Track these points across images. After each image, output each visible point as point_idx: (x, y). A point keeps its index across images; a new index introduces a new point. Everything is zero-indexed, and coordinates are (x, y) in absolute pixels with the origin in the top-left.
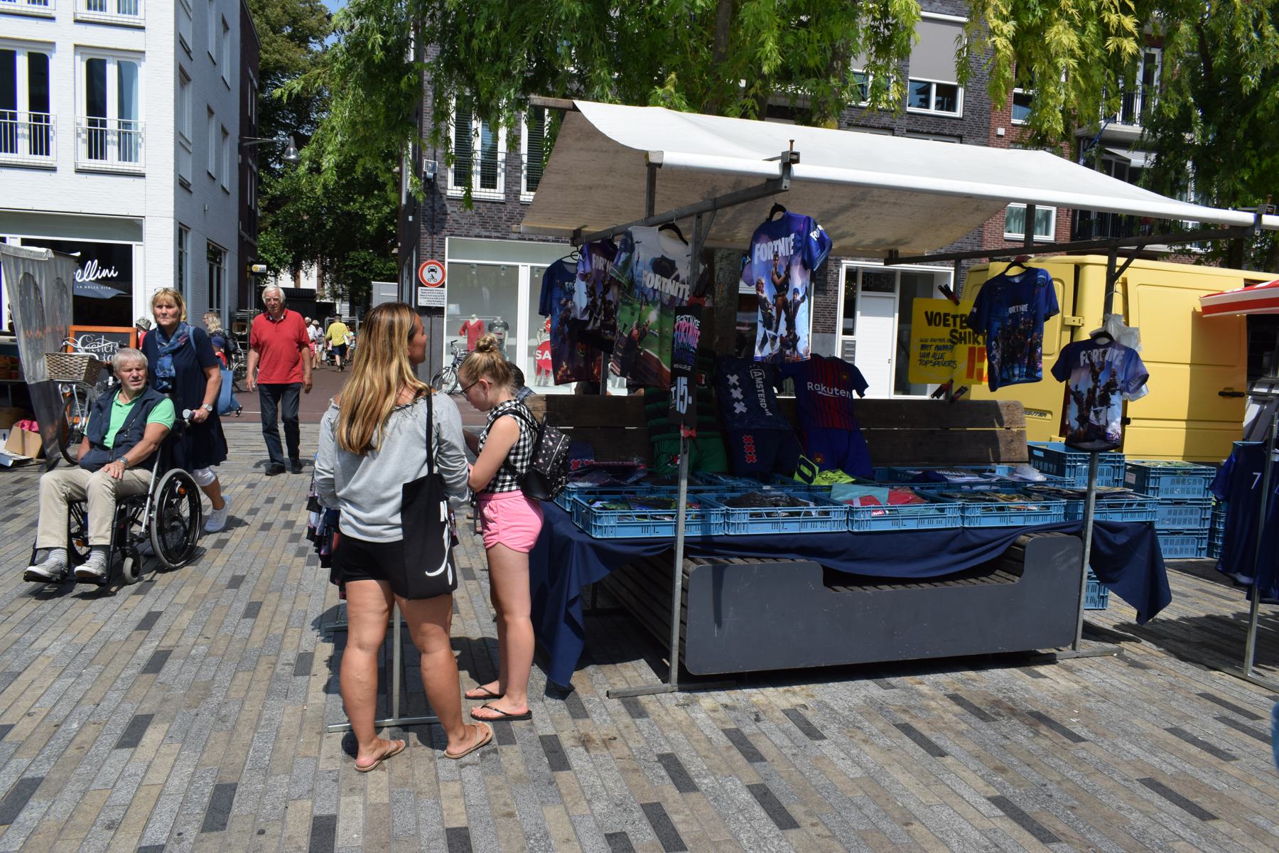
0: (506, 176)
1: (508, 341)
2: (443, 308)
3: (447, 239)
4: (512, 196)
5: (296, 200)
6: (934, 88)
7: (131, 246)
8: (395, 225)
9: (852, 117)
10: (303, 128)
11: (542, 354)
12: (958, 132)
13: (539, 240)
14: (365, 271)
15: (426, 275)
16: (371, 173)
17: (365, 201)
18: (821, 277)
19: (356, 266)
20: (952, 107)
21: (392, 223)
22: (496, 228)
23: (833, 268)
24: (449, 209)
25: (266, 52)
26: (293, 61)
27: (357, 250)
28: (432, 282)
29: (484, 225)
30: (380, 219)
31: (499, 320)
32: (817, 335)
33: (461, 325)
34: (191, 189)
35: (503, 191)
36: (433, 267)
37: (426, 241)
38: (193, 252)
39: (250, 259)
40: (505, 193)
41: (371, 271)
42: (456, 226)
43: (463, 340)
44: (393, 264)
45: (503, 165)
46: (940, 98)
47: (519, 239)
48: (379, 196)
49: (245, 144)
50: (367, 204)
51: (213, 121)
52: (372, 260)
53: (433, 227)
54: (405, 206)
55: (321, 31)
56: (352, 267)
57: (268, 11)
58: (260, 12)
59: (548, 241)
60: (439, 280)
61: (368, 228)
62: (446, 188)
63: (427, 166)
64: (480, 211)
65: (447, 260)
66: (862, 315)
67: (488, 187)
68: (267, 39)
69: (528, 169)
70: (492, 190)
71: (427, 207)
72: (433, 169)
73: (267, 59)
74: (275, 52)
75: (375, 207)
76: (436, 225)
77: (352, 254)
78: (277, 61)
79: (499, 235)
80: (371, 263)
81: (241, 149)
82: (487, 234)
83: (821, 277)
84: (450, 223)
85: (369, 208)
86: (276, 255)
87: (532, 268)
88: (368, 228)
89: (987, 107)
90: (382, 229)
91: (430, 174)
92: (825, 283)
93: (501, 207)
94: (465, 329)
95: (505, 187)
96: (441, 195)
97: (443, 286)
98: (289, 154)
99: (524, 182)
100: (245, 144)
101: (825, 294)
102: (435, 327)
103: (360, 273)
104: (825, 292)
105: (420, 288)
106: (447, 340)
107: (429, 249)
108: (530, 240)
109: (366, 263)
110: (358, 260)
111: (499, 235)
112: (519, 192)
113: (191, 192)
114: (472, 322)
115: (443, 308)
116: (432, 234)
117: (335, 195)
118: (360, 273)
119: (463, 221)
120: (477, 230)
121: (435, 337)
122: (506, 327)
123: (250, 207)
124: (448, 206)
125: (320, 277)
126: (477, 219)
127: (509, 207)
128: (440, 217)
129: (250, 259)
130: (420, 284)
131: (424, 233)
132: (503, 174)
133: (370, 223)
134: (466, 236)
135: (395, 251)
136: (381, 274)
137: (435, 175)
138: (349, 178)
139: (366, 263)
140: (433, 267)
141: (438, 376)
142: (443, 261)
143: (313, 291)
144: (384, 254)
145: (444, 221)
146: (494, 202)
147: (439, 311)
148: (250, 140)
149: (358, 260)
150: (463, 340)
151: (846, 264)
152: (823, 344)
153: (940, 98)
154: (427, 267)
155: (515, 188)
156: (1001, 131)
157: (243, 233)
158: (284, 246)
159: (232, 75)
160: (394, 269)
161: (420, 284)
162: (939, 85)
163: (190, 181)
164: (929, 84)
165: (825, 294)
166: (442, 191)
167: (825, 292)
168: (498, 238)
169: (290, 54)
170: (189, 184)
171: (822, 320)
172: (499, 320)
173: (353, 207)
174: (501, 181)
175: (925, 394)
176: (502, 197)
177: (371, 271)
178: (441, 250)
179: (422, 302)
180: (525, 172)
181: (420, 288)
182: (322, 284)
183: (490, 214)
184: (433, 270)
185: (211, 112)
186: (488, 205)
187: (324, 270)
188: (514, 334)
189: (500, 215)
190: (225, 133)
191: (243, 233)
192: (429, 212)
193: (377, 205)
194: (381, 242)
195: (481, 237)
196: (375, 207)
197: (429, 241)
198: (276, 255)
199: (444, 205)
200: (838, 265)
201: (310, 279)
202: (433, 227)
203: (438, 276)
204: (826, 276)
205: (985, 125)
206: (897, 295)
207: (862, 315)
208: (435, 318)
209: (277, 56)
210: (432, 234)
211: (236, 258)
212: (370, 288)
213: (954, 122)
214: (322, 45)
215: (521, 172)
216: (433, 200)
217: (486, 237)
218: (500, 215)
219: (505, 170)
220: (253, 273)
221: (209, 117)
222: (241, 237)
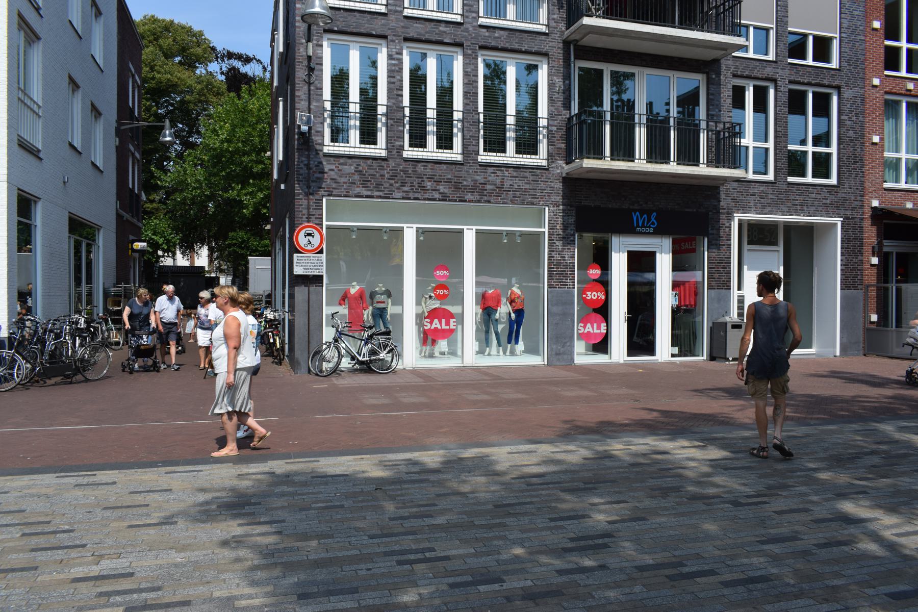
0: (387, 131)
1: (391, 310)
2: (322, 276)
3: (324, 200)
4: (394, 152)
5: (182, 191)
6: (811, 40)
7: (629, 354)
8: (268, 208)
9: (737, 68)
10: (192, 137)
11: (431, 323)
12: (836, 83)
13: (425, 199)
14: (242, 249)
15: (302, 240)
16: (247, 166)
17: (242, 189)
18: (714, 232)
19: (234, 245)
20: (827, 59)
21: (265, 207)
22: (378, 186)
23: (725, 222)
24: (327, 167)
25: (159, 73)
26: (182, 80)
27: (235, 231)
28: (309, 248)
29: (365, 184)
30: (254, 203)
31: (381, 288)
32: (713, 291)
33: (341, 294)
34: (41, 155)
35: (384, 146)
36: (309, 230)
37: (301, 203)
38: (43, 224)
39: (131, 237)
40: (387, 149)
41: (248, 248)
42: (334, 185)
43: (344, 310)
44: (267, 242)
45: (384, 119)
46: (680, 109)
47: (404, 198)
48: (254, 184)
49: (123, 128)
50: (244, 192)
51: (79, 95)
52: (249, 239)
53: (309, 187)
54: (276, 180)
55: (206, 58)
56: (229, 246)
57: (161, 41)
58: (155, 42)
59: (434, 200)
60: (316, 245)
61: (245, 211)
62: (323, 145)
63: (302, 119)
64: (360, 168)
65: (325, 223)
66: (749, 269)
67: (369, 143)
68: (160, 63)
69: (410, 123)
70: (373, 146)
71: (302, 165)
72: (308, 122)
73: (160, 78)
74: (166, 73)
75: (251, 194)
76: (313, 184)
77: (231, 234)
78: (169, 80)
79: (381, 194)
80: (248, 242)
81: (119, 132)
82: (369, 193)
83: (714, 232)
84: (326, 184)
85: (246, 195)
86: (165, 237)
87: (418, 230)
88: (245, 211)
89: (862, 57)
90: (257, 211)
91: (304, 128)
92: (718, 237)
93: (383, 163)
94: (344, 298)
95: (387, 142)
96: (317, 152)
97: (321, 252)
98: (165, 136)
99: (407, 137)
100: (123, 128)
101: (719, 249)
102: (312, 297)
103: (238, 250)
104: (718, 247)
105: (295, 255)
106: (326, 311)
107: (305, 212)
108: (415, 199)
109: (243, 241)
110: (236, 239)
111: (381, 194)
112: (402, 148)
113: (41, 159)
114: (353, 291)
115: (322, 276)
116: (308, 194)
117: (215, 184)
118: (238, 250)
119: (343, 180)
120: (358, 190)
121: (312, 312)
122: (388, 294)
123: (132, 190)
124: (324, 163)
125: (210, 256)
126: (356, 177)
127: (392, 163)
128: (317, 175)
129: (131, 237)
130: (295, 250)
131: (299, 195)
132: (384, 129)
133: (246, 207)
134: (345, 196)
135: (268, 227)
136: (256, 250)
137: (310, 128)
138: (228, 170)
139: (243, 241)
140: (309, 230)
141: (318, 352)
142: (322, 225)
143: (203, 268)
144: (260, 234)
145: (320, 180)
146: (375, 159)
147: (318, 279)
148: (130, 124)
149: (236, 239)
150: (344, 310)
151: (738, 216)
152: (719, 300)
153: (680, 109)
154: (303, 231)
155: (397, 143)
156: (876, 82)
157: (121, 212)
158: (173, 230)
159: (105, 58)
160: (267, 246)
161: (295, 250)
162: (816, 38)
163: (40, 148)
164: (805, 36)
165: (719, 249)
166: (318, 147)
167: (718, 247)
168: (380, 197)
169: (179, 75)
170: (39, 151)
171: (716, 276)
172: (381, 288)
173: (232, 194)
174: (382, 136)
175: (810, 347)
176: (383, 154)
177: (248, 248)
178: (318, 212)
179: (298, 270)
180: (407, 127)
181: (295, 255)
182: (211, 262)
183: (372, 172)
184: (309, 235)
185: (74, 84)
186: (369, 162)
187: (211, 251)
188: (400, 302)
189: (382, 172)
190: (96, 112)
191: (121, 212)
192: (304, 171)
193: (252, 192)
194: (255, 222)
195: (362, 197)
196: (251, 194)
197: (305, 202)
198: (165, 237)
199: (321, 163)
200: (730, 217)
201: (202, 259)
202: (309, 187)
203: (316, 241)
204: (719, 230)
205: (861, 75)
206: (781, 248)
207: (749, 269)
208: (313, 288)
209: (169, 76)
210: (308, 194)
211: (113, 236)
212: (247, 262)
213: (832, 72)
214: (206, 70)
215: (404, 126)
216: (308, 157)
217: (367, 197)
218: (382, 172)
219: (386, 125)
220: (134, 251)
221: (73, 91)
222: (119, 217)
